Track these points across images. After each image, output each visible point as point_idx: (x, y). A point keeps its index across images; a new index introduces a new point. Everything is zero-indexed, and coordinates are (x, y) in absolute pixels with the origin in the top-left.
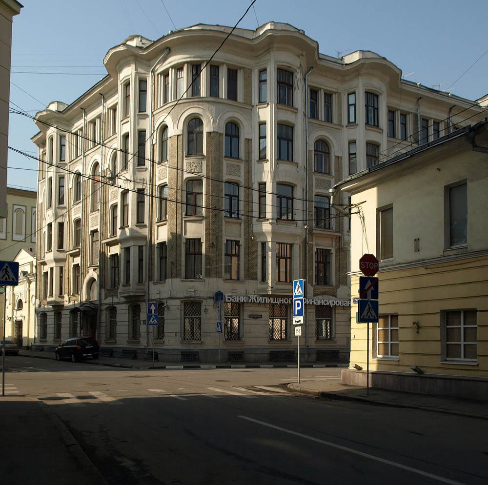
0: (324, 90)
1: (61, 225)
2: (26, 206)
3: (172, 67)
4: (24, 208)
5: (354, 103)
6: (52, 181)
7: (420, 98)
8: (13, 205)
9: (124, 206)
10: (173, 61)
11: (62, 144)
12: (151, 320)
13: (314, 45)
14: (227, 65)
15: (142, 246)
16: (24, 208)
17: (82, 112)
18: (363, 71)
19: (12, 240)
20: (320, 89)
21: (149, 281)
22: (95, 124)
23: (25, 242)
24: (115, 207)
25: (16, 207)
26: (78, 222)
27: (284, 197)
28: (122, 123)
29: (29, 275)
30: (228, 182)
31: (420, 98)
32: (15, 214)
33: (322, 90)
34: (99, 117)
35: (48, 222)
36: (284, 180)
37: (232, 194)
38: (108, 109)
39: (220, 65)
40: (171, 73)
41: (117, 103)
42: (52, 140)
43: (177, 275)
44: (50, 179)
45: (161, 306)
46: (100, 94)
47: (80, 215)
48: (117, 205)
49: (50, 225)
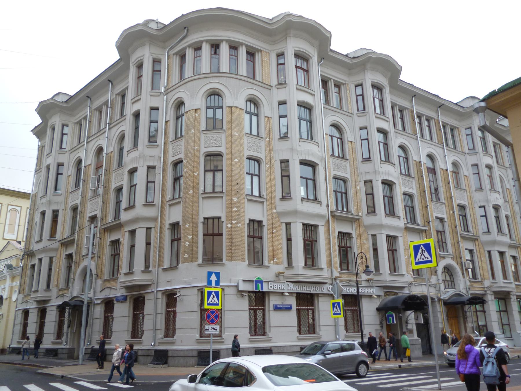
0: (334, 80)
1: (55, 214)
2: (21, 207)
3: (189, 46)
4: (19, 209)
5: (361, 93)
6: (49, 169)
7: (415, 96)
8: (9, 205)
9: (133, 186)
10: (190, 41)
11: (60, 172)
12: (210, 299)
13: (329, 35)
14: (246, 46)
15: (150, 228)
16: (19, 209)
17: (87, 101)
18: (369, 66)
19: (3, 239)
20: (331, 79)
21: (158, 267)
22: (101, 112)
23: (9, 205)
24: (119, 190)
25: (10, 207)
26: (75, 209)
27: (337, 157)
28: (133, 101)
29: (15, 268)
30: (249, 158)
31: (415, 96)
32: (9, 214)
33: (332, 81)
34: (106, 103)
35: (41, 210)
36: (307, 159)
37: (253, 173)
38: (116, 95)
39: (239, 46)
40: (189, 54)
41: (127, 88)
42: (53, 129)
43: (193, 258)
44: (48, 167)
45: (171, 297)
46: (109, 80)
47: (78, 202)
48: (122, 188)
49: (43, 214)
